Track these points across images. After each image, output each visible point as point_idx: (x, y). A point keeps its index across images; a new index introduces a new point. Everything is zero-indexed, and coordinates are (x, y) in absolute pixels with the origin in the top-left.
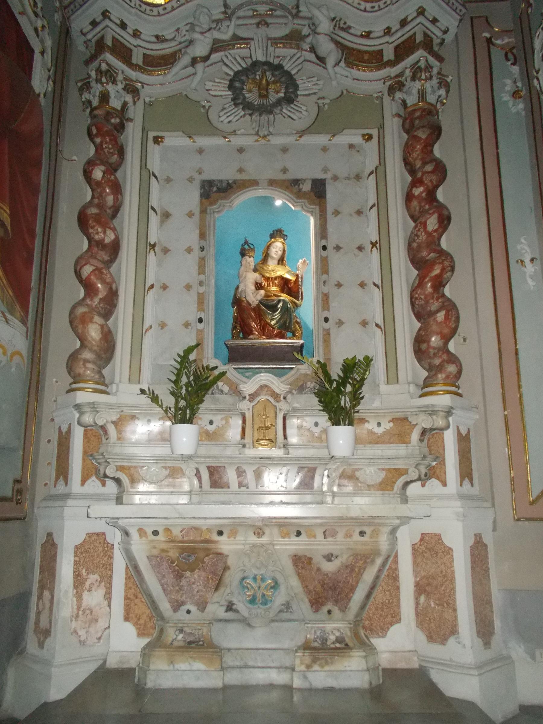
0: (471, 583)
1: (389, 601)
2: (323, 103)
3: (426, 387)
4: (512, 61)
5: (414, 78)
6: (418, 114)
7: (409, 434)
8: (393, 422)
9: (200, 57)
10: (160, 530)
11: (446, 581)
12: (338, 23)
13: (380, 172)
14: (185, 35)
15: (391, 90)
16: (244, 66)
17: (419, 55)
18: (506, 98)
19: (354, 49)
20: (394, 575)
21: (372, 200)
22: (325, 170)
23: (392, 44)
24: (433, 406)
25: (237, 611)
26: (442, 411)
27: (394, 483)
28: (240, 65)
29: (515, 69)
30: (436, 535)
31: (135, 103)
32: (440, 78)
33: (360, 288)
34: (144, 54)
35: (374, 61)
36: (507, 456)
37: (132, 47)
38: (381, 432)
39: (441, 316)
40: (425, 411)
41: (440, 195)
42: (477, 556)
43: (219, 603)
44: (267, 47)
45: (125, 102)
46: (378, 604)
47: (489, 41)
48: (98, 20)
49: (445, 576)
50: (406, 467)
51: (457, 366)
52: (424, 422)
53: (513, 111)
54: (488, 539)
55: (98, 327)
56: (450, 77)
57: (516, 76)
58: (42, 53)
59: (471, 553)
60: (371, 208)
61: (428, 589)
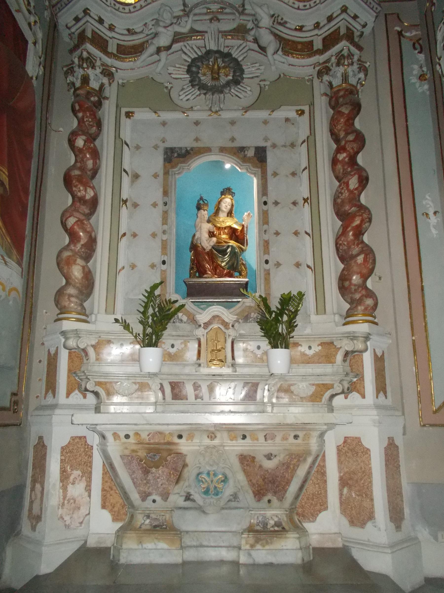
0: (385, 477)
1: (318, 492)
2: (264, 85)
3: (348, 317)
4: (419, 50)
6: (342, 93)
7: (335, 356)
8: (322, 346)
9: (164, 47)
10: (131, 434)
11: (365, 476)
12: (276, 19)
13: (310, 141)
14: (151, 29)
15: (320, 74)
16: (200, 54)
17: (343, 45)
18: (414, 80)
19: (289, 40)
20: (322, 471)
21: (304, 164)
22: (266, 139)
23: (321, 36)
24: (354, 332)
25: (194, 501)
26: (362, 337)
27: (322, 395)
28: (196, 53)
29: (421, 57)
30: (356, 438)
31: (110, 84)
32: (360, 64)
33: (294, 236)
34: (118, 44)
35: (306, 50)
36: (415, 374)
37: (108, 39)
38: (312, 354)
39: (360, 259)
40: (348, 337)
41: (360, 159)
42: (390, 456)
43: (179, 494)
44: (218, 39)
45: (102, 83)
46: (309, 495)
47: (400, 34)
48: (80, 16)
49: (364, 472)
50: (332, 383)
51: (373, 300)
52: (347, 345)
54: (399, 442)
55: (80, 268)
56: (368, 63)
58: (35, 43)
59: (385, 453)
60: (304, 170)
61: (350, 482)
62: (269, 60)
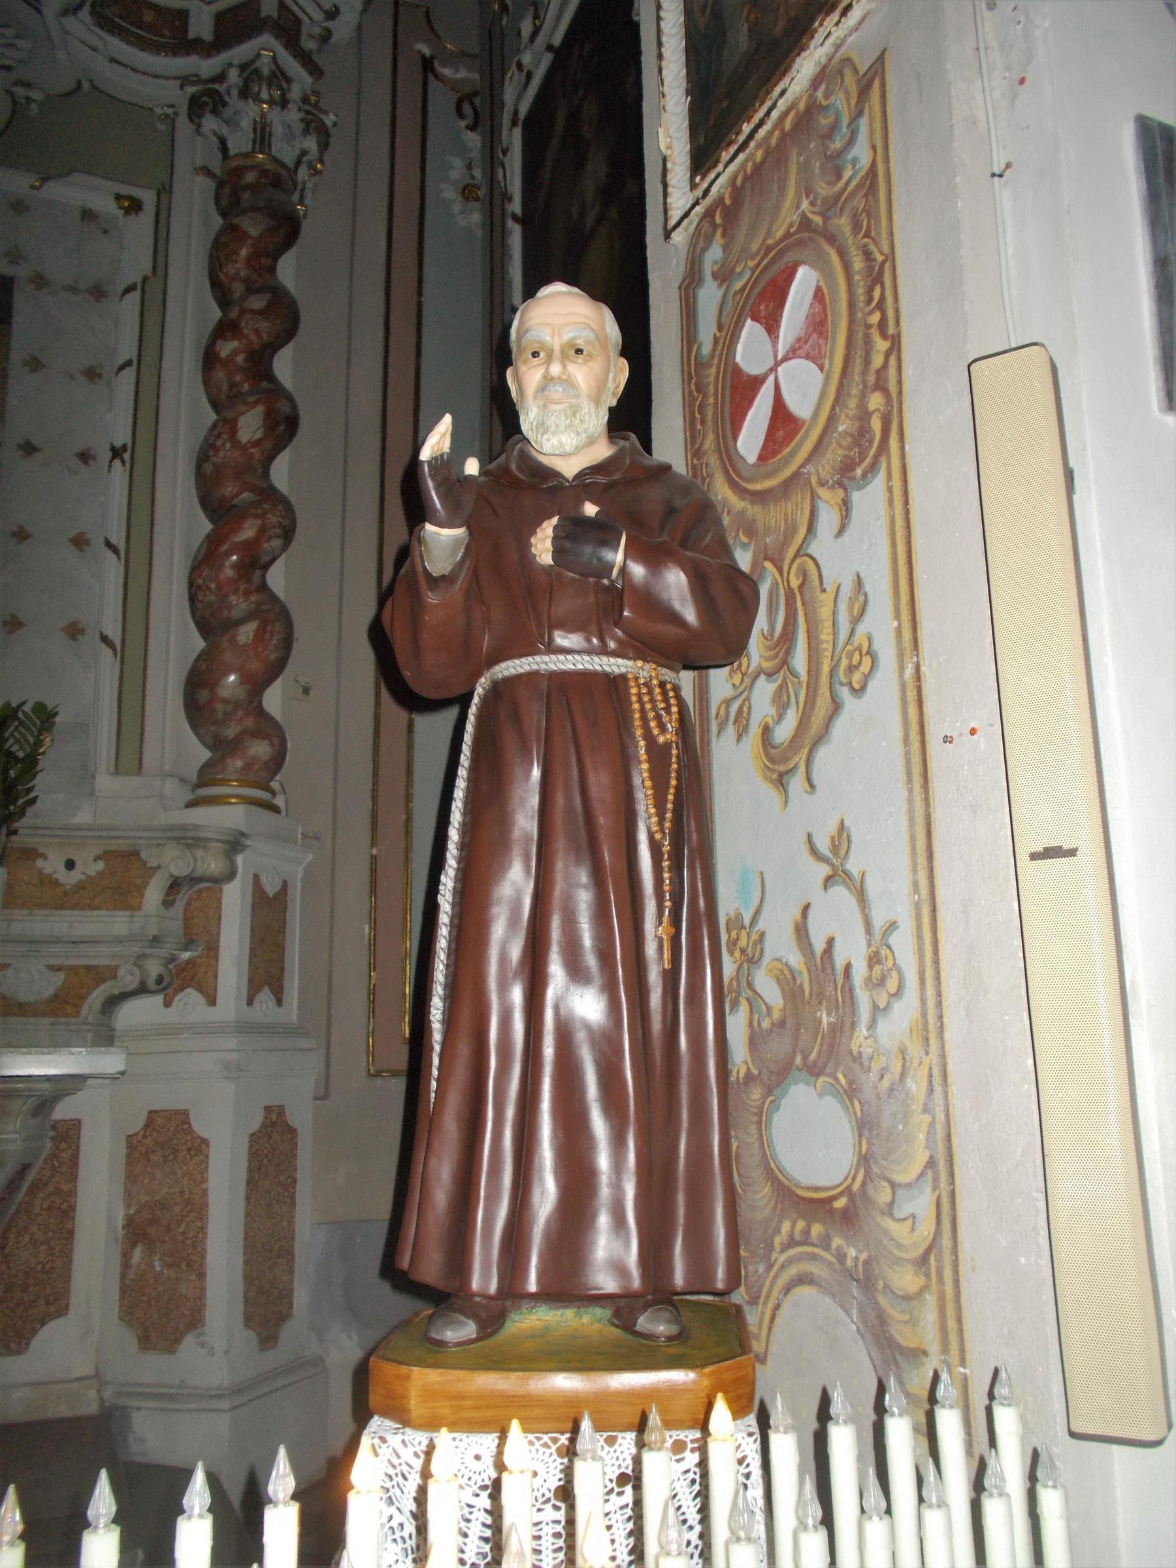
0: (242, 1214)
1: (43, 1267)
2: (27, 98)
3: (204, 785)
4: (469, 121)
5: (245, 93)
6: (250, 177)
7: (141, 890)
8: (106, 861)
11: (188, 1212)
13: (152, 291)
15: (196, 107)
17: (265, 48)
18: (450, 193)
20: (64, 1206)
21: (127, 350)
22: (15, 256)
24: (196, 827)
26: (218, 841)
27: (83, 998)
29: (474, 140)
30: (178, 1112)
32: (308, 112)
33: (73, 548)
36: (366, 941)
38: (74, 882)
39: (246, 633)
40: (174, 839)
41: (283, 365)
42: (266, 1156)
46: (16, 1276)
47: (427, 65)
49: (188, 1202)
50: (114, 963)
51: (272, 745)
52: (176, 862)
54: (301, 1117)
56: (332, 117)
59: (251, 1147)
60: (122, 368)
61: (152, 1231)
62: (45, 25)
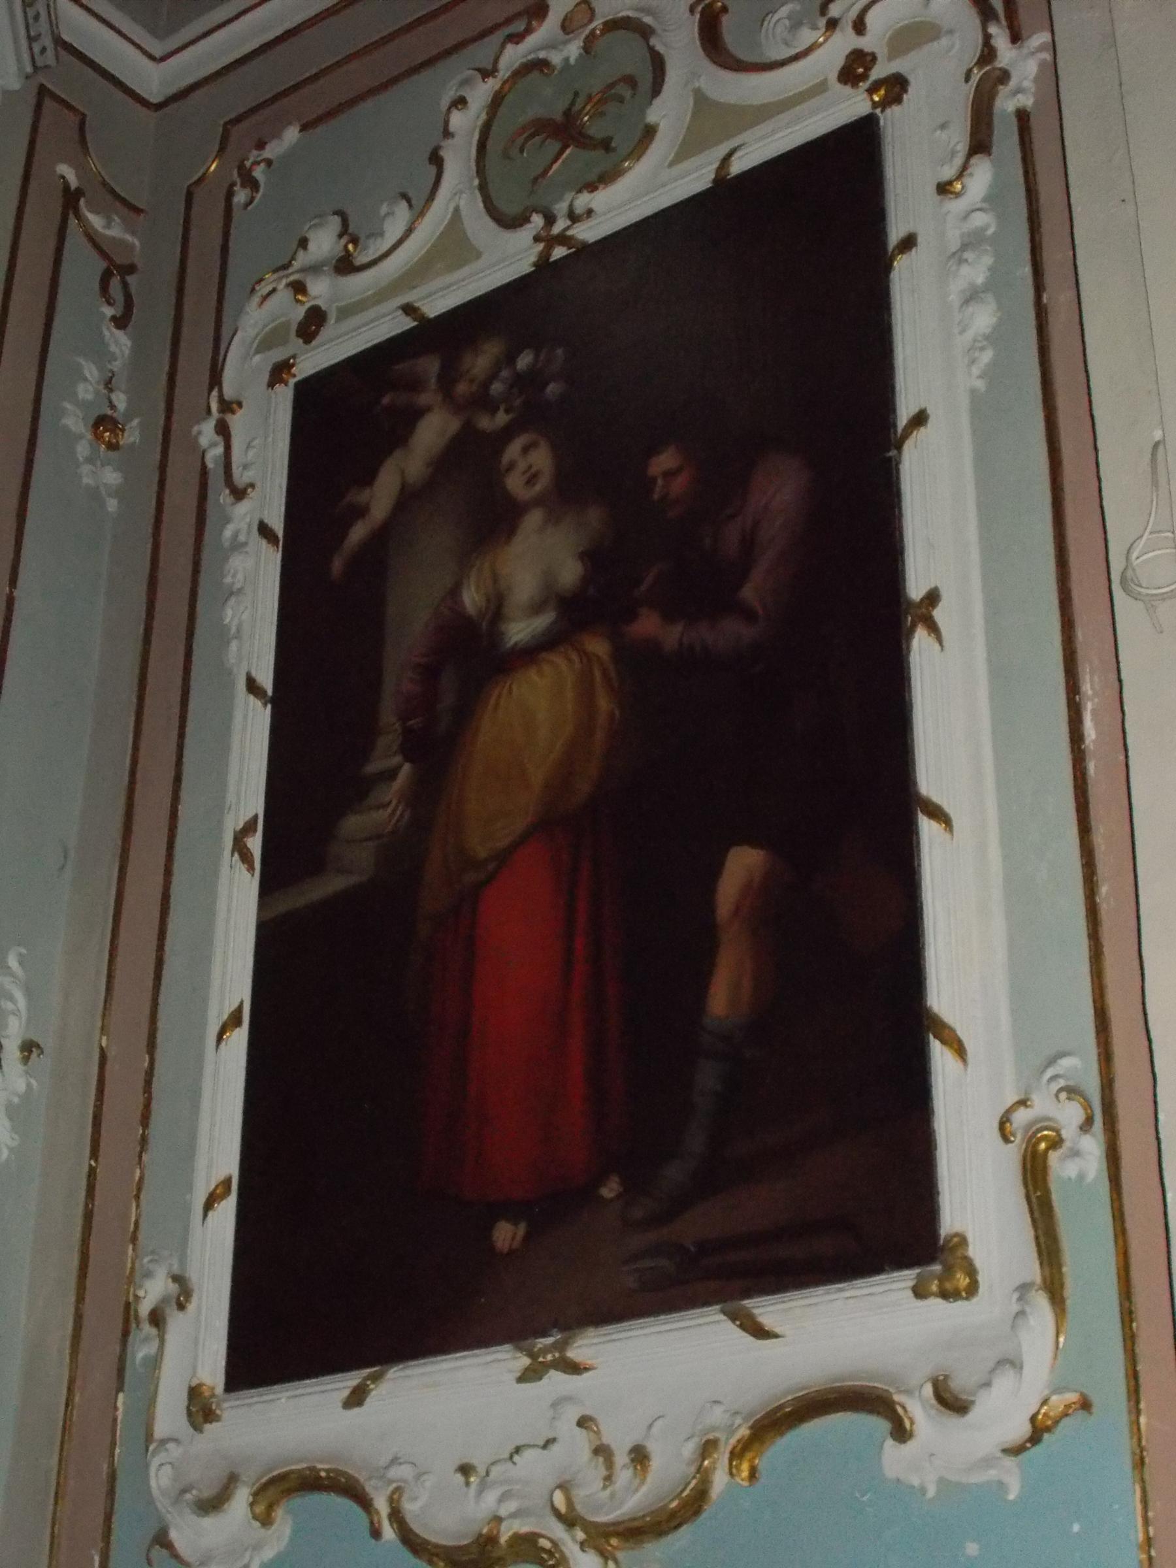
18: (75, 422)
29: (120, 343)
47: (71, 199)
53: (85, 480)
57: (116, 366)
